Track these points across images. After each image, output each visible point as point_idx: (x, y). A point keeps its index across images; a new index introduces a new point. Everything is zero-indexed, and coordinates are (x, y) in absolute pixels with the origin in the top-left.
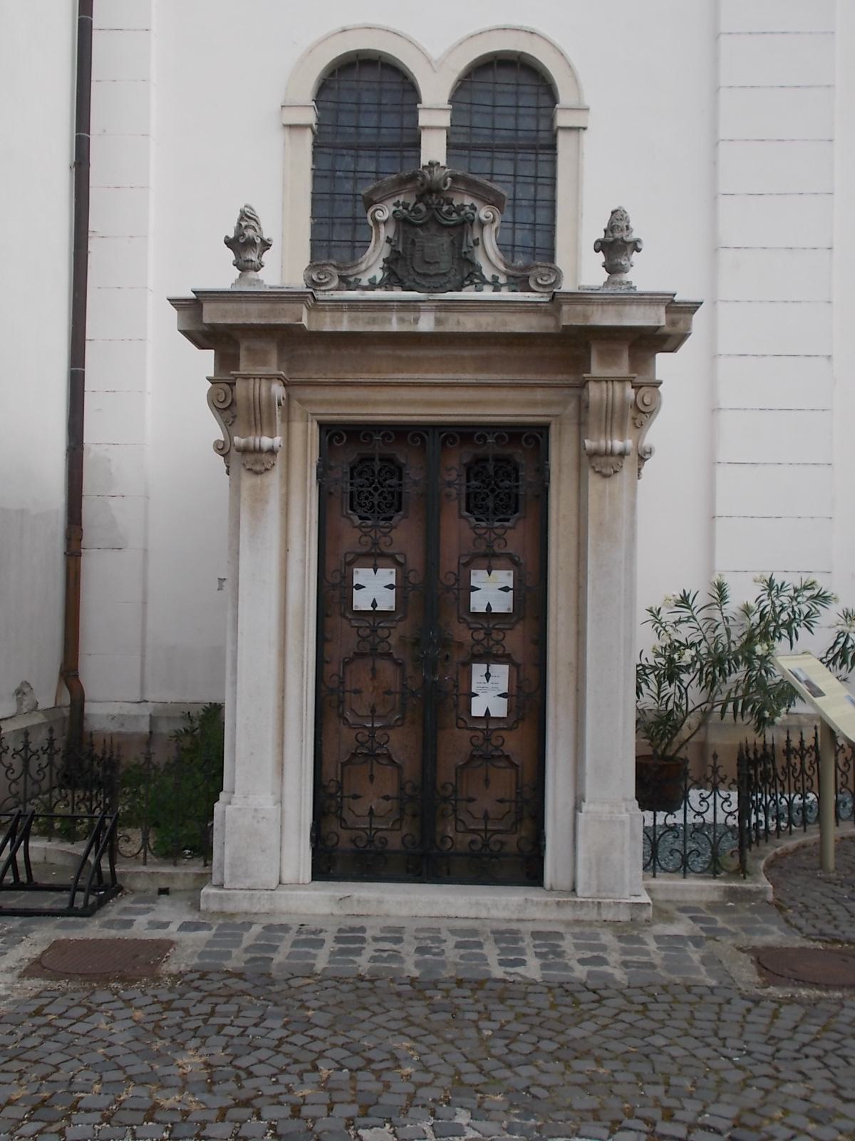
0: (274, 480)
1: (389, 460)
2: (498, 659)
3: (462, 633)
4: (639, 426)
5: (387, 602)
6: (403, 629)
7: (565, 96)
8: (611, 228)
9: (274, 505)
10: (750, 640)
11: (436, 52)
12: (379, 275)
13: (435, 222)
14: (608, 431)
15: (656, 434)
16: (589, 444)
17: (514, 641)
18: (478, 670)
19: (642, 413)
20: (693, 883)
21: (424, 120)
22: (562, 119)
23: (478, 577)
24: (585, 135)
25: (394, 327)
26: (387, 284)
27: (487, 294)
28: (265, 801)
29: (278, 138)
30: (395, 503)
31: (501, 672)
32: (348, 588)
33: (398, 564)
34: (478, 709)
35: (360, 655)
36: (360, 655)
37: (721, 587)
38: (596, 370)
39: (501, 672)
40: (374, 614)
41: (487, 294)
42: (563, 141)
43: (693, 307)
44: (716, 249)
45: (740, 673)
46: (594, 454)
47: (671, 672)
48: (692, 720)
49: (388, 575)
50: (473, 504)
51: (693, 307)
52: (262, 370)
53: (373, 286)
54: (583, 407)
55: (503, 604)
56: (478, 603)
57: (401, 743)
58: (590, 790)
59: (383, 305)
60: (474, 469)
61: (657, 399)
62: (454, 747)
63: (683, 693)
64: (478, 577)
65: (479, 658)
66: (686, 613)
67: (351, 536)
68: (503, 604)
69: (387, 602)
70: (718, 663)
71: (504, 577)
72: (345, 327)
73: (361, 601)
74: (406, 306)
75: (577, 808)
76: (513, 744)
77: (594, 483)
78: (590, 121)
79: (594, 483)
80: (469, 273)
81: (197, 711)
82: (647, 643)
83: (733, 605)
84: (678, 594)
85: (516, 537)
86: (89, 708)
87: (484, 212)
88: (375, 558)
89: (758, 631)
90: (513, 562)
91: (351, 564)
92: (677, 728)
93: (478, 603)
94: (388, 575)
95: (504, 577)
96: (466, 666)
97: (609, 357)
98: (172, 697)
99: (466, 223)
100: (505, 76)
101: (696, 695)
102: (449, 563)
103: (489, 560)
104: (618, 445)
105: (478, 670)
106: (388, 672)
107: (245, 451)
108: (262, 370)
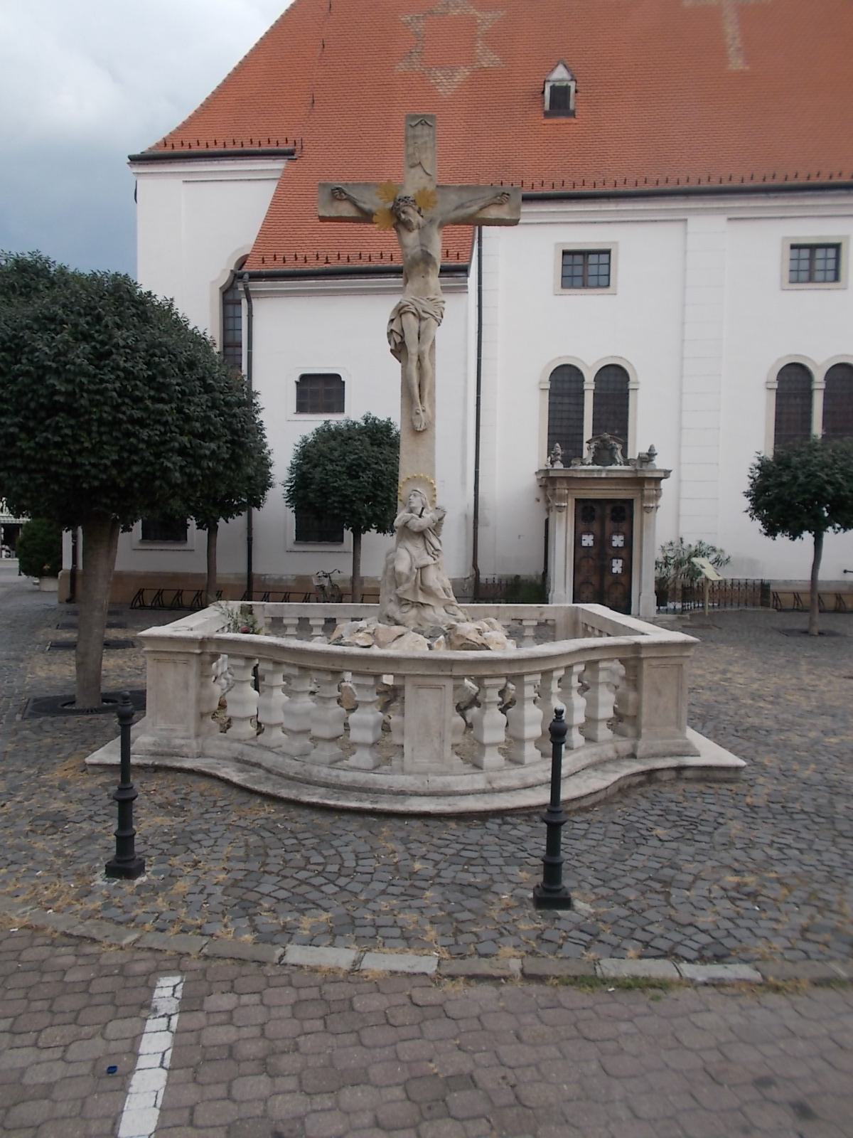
0: (564, 513)
1: (592, 508)
2: (620, 558)
3: (611, 552)
4: (657, 500)
5: (591, 544)
6: (594, 552)
7: (632, 378)
8: (650, 450)
9: (564, 520)
10: (690, 557)
11: (590, 364)
12: (591, 461)
13: (605, 448)
14: (649, 502)
15: (661, 502)
16: (644, 505)
17: (624, 554)
18: (614, 561)
19: (657, 497)
20: (669, 615)
21: (585, 387)
22: (631, 386)
23: (614, 537)
24: (638, 391)
25: (596, 476)
26: (593, 464)
27: (618, 467)
28: (562, 592)
29: (538, 392)
30: (593, 518)
31: (620, 561)
32: (625, 541)
33: (593, 534)
34: (614, 571)
35: (584, 557)
36: (584, 557)
37: (681, 539)
38: (646, 487)
39: (620, 561)
40: (588, 547)
41: (618, 467)
42: (631, 393)
43: (670, 471)
44: (681, 429)
45: (686, 566)
46: (645, 507)
47: (666, 564)
48: (671, 580)
49: (591, 537)
50: (614, 519)
51: (670, 471)
52: (563, 487)
53: (589, 464)
54: (643, 497)
55: (621, 544)
56: (614, 544)
57: (594, 579)
58: (643, 590)
59: (593, 471)
60: (613, 510)
61: (661, 493)
62: (608, 580)
63: (669, 570)
64: (614, 537)
65: (615, 558)
66: (671, 547)
67: (582, 527)
68: (621, 544)
69: (591, 544)
70: (679, 564)
71: (621, 537)
72: (583, 476)
73: (584, 544)
74: (599, 471)
75: (640, 595)
76: (623, 580)
77: (645, 514)
78: (640, 387)
79: (645, 514)
80: (613, 461)
81: (513, 577)
82: (660, 556)
83: (685, 545)
84: (669, 541)
85: (624, 527)
86: (481, 576)
87: (618, 446)
88: (588, 533)
89: (212, 428)
90: (624, 534)
91: (582, 534)
92: (666, 582)
93: (614, 544)
94: (591, 537)
95: (621, 537)
96: (611, 560)
97: (649, 484)
98: (504, 573)
99: (613, 449)
100: (612, 370)
101: (672, 572)
102: (607, 535)
103: (618, 533)
104: (651, 505)
105: (614, 561)
106: (591, 561)
107: (558, 506)
108: (563, 487)
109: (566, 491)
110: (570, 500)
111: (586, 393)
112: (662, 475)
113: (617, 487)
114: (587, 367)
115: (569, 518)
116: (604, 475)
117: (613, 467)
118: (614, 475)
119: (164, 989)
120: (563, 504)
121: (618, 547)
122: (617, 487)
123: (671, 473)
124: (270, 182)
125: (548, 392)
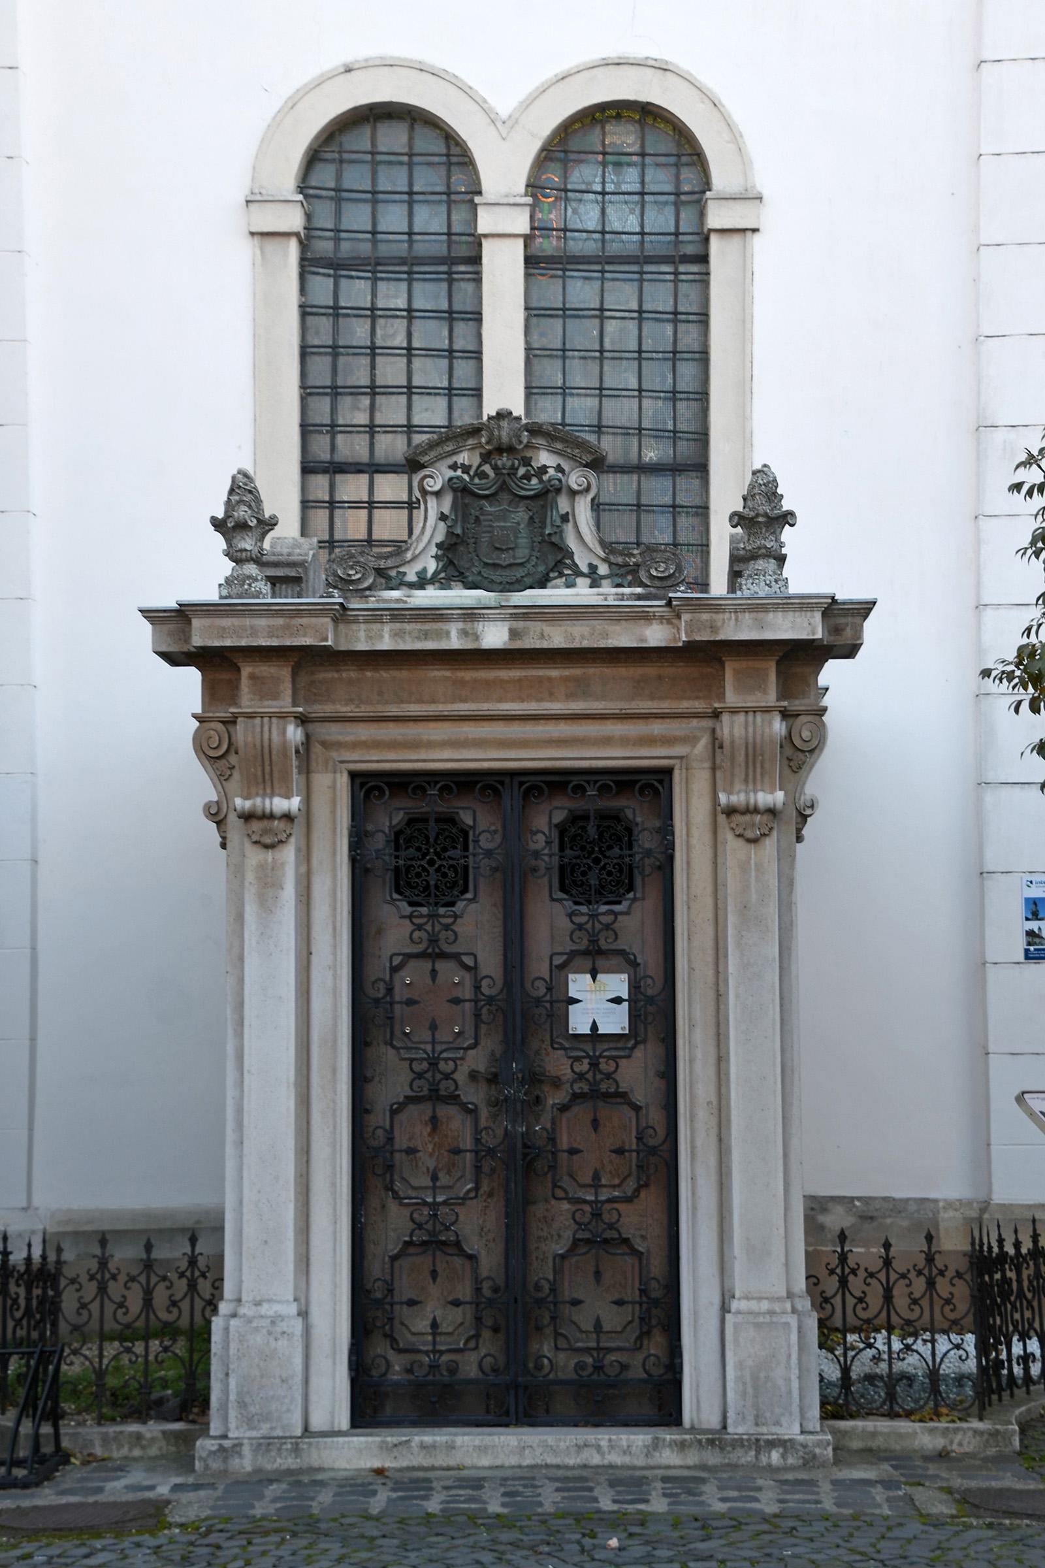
0: (289, 854)
7: (722, 178)
11: (504, 106)
12: (432, 566)
21: (486, 222)
23: (579, 984)
24: (757, 240)
26: (442, 580)
27: (582, 593)
29: (246, 250)
41: (582, 593)
43: (865, 609)
51: (865, 609)
52: (271, 706)
53: (422, 583)
56: (579, 1022)
64: (579, 984)
68: (615, 1022)
71: (617, 984)
72: (386, 643)
74: (470, 614)
78: (768, 218)
95: (617, 984)
102: (539, 967)
108: (271, 706)
109: (294, 733)
110: (321, 780)
111: (489, 249)
112: (811, 628)
113: (665, 706)
114: (493, 118)
115: (321, 887)
116: (494, 636)
117: (555, 595)
118: (557, 637)
119: (1021, 1238)
120: (280, 804)
121: (595, 1033)
122: (665, 706)
123: (870, 626)
124: (519, 209)
125: (293, 247)
